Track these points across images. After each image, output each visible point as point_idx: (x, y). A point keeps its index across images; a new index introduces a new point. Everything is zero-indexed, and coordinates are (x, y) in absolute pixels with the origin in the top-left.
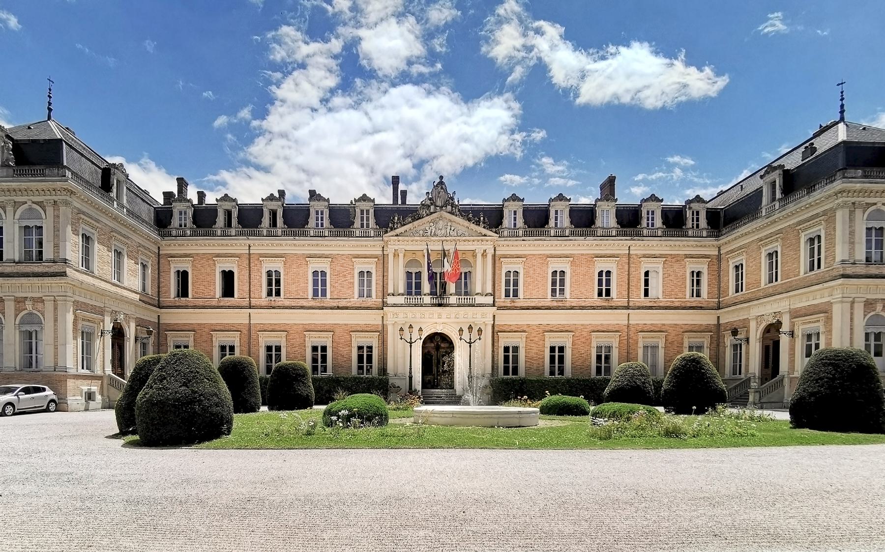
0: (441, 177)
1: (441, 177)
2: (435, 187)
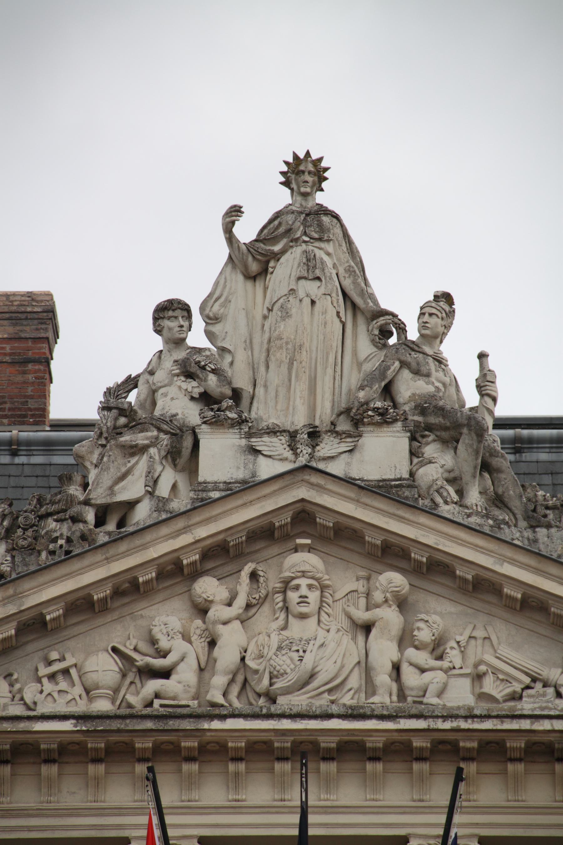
0: (304, 173)
1: (304, 173)
2: (253, 261)
